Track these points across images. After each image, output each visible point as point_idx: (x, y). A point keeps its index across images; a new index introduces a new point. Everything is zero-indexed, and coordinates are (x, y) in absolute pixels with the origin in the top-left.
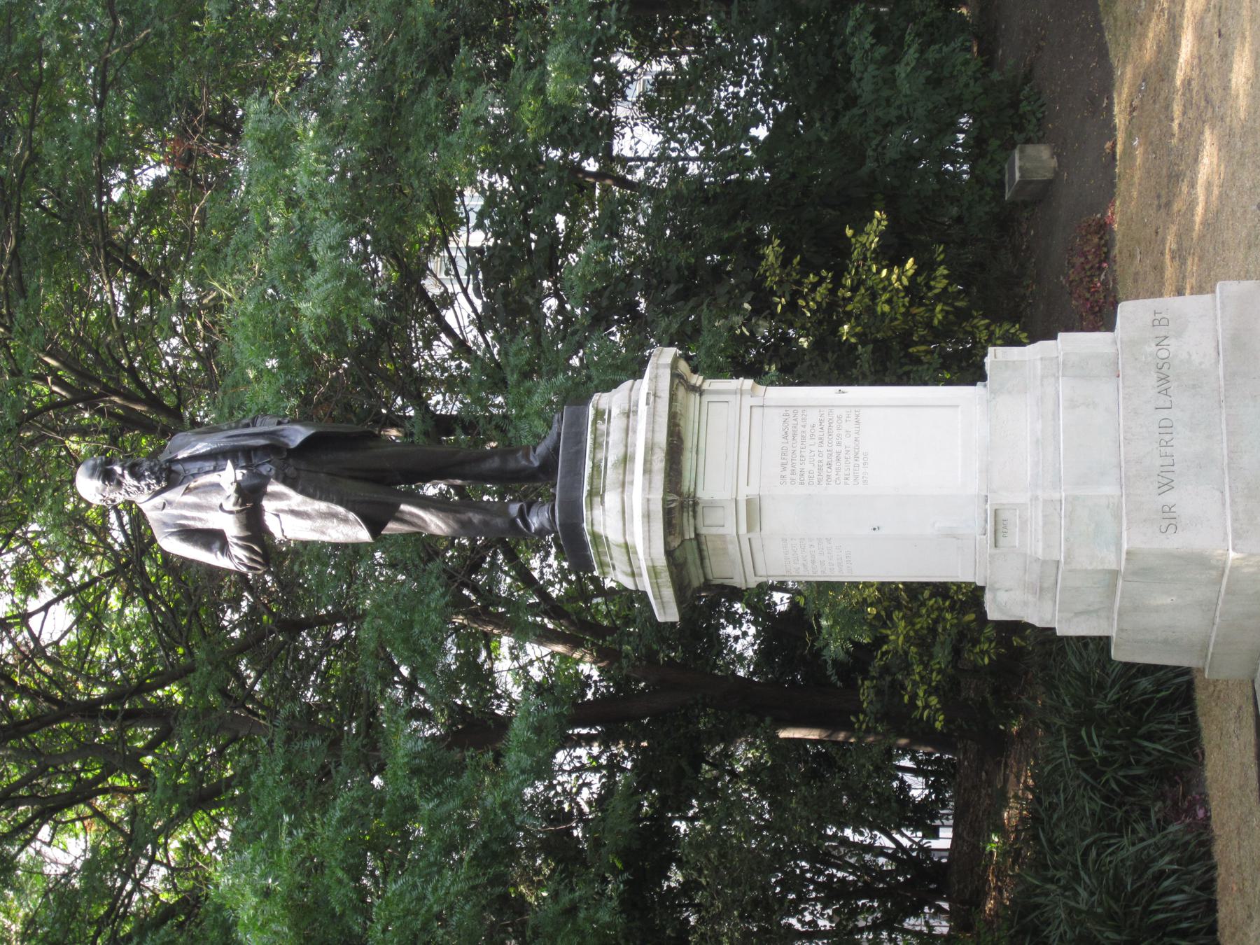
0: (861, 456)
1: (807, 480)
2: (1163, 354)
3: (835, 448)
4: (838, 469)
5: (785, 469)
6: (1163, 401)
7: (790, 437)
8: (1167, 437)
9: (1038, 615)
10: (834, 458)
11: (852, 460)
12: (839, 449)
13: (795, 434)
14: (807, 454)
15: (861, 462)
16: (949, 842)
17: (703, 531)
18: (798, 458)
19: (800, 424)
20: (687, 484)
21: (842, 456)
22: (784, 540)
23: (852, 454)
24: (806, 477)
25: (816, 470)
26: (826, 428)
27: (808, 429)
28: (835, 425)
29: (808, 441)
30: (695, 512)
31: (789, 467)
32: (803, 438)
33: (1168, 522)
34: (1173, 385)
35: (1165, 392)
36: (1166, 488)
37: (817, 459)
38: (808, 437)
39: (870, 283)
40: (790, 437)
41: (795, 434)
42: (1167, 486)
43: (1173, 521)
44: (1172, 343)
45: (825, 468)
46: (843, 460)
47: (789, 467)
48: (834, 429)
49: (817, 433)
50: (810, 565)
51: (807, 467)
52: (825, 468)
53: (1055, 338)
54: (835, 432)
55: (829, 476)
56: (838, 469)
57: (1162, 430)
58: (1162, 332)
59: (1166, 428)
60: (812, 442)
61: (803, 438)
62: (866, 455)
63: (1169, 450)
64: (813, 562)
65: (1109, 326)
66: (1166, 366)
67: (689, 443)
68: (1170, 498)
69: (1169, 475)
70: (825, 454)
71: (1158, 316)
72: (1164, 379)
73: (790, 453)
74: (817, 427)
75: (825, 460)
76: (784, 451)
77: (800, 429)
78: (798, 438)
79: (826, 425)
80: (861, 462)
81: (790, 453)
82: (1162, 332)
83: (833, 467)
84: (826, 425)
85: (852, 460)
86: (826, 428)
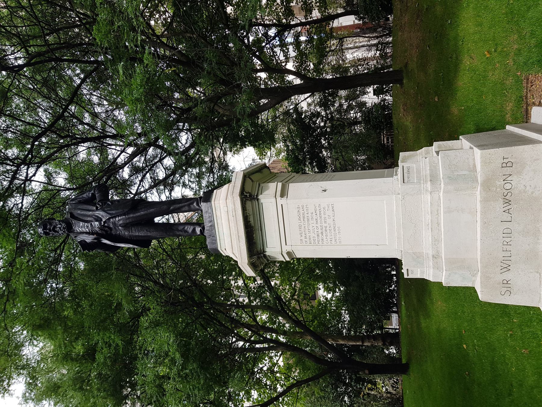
1: (312, 242)
2: (508, 186)
3: (324, 225)
4: (326, 235)
6: (506, 217)
7: (302, 220)
8: (508, 240)
10: (324, 230)
11: (332, 231)
12: (325, 225)
13: (304, 218)
14: (311, 228)
15: (337, 232)
18: (307, 230)
19: (306, 212)
20: (259, 247)
21: (328, 228)
23: (332, 228)
24: (312, 239)
26: (318, 214)
27: (310, 215)
28: (322, 212)
29: (311, 222)
32: (308, 220)
33: (506, 289)
34: (513, 206)
35: (508, 211)
36: (505, 270)
37: (316, 230)
38: (310, 219)
39: (216, 108)
40: (302, 220)
41: (304, 218)
42: (507, 269)
43: (509, 289)
44: (514, 179)
45: (320, 235)
46: (328, 231)
48: (322, 214)
49: (315, 217)
51: (312, 235)
52: (320, 235)
54: (323, 216)
55: (322, 239)
56: (326, 235)
57: (504, 235)
58: (508, 171)
59: (508, 234)
60: (312, 222)
61: (308, 220)
63: (508, 248)
66: (509, 194)
68: (507, 276)
70: (320, 227)
72: (508, 202)
73: (303, 227)
74: (314, 214)
76: (300, 227)
77: (306, 215)
78: (306, 219)
79: (318, 212)
80: (337, 232)
81: (303, 227)
83: (324, 234)
84: (318, 212)
85: (332, 231)
86: (318, 214)
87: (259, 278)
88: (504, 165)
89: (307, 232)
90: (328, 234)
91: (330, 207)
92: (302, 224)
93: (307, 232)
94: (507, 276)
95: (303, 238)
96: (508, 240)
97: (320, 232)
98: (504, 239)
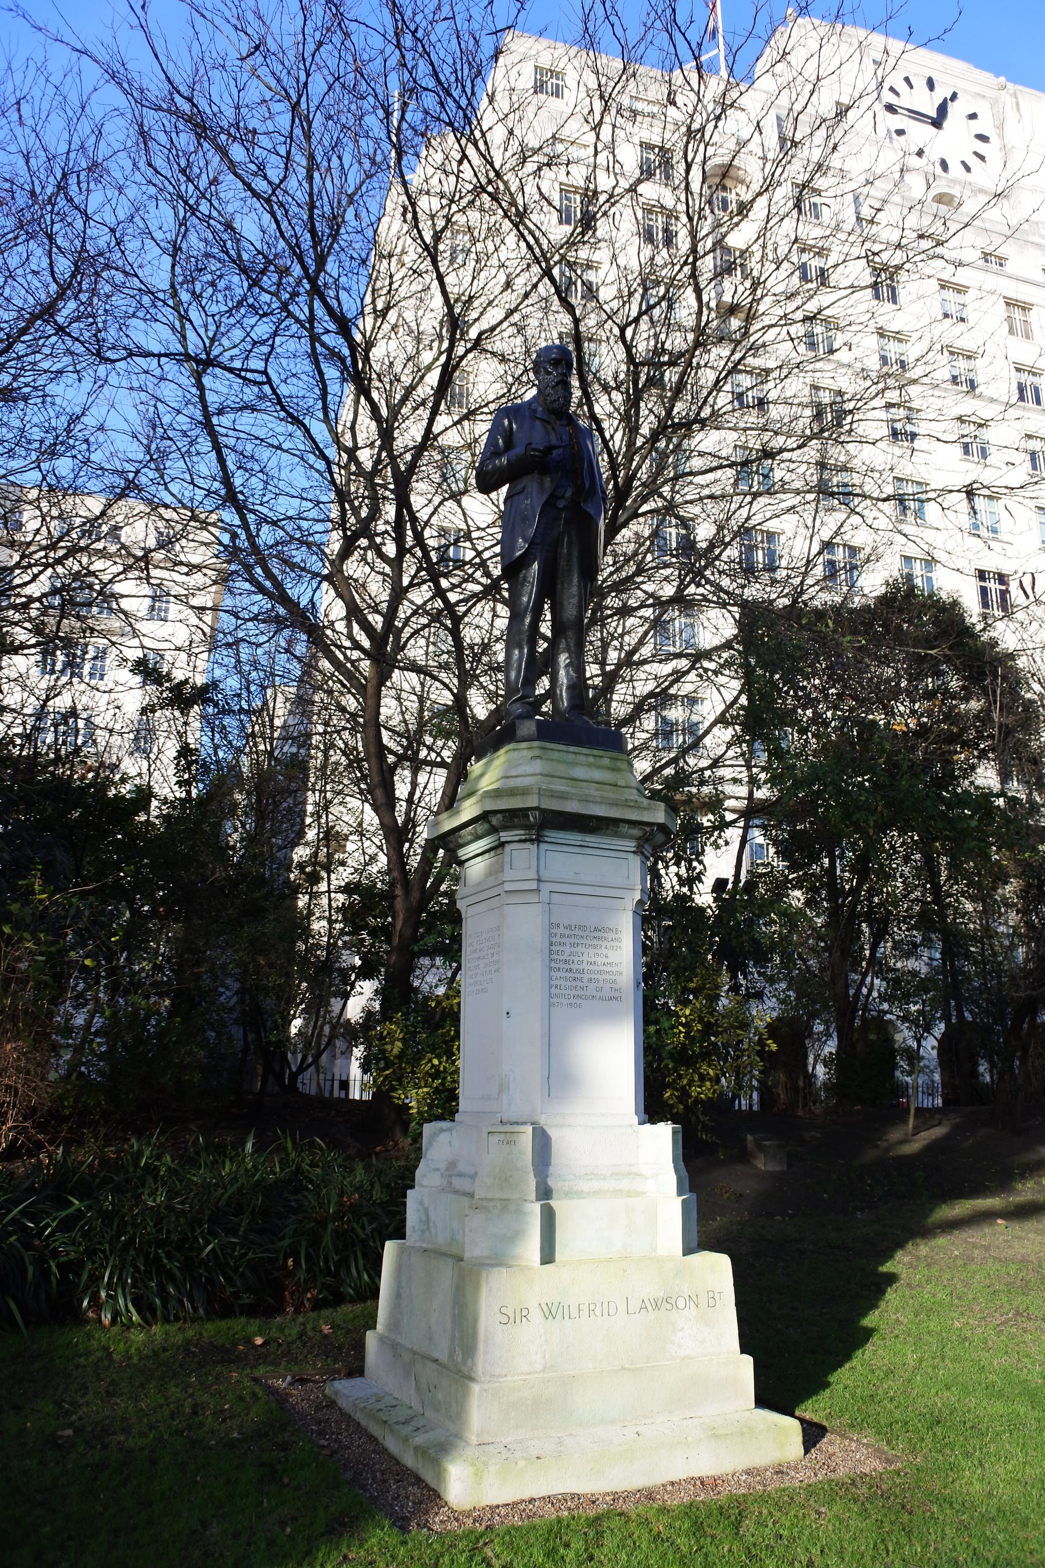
0: (579, 1001)
2: (681, 1303)
5: (566, 928)
6: (635, 1304)
8: (598, 1311)
9: (427, 1176)
11: (574, 992)
15: (572, 1001)
16: (357, 1097)
17: (508, 848)
20: (552, 835)
21: (579, 984)
22: (498, 929)
23: (581, 993)
25: (565, 957)
30: (525, 841)
31: (568, 932)
45: (567, 966)
46: (574, 984)
47: (568, 932)
50: (476, 955)
52: (567, 966)
53: (652, 1109)
62: (580, 1005)
64: (478, 958)
65: (763, 1400)
66: (669, 1307)
67: (591, 839)
68: (536, 1315)
69: (559, 1316)
71: (717, 1296)
73: (581, 933)
75: (574, 967)
80: (572, 1001)
81: (581, 933)
82: (703, 1300)
83: (568, 975)
85: (574, 992)
87: (969, 621)
88: (711, 1295)
89: (573, 940)
90: (568, 984)
91: (616, 994)
92: (588, 933)
93: (573, 940)
94: (536, 1315)
95: (562, 930)
96: (598, 1311)
97: (572, 966)
98: (599, 1305)
